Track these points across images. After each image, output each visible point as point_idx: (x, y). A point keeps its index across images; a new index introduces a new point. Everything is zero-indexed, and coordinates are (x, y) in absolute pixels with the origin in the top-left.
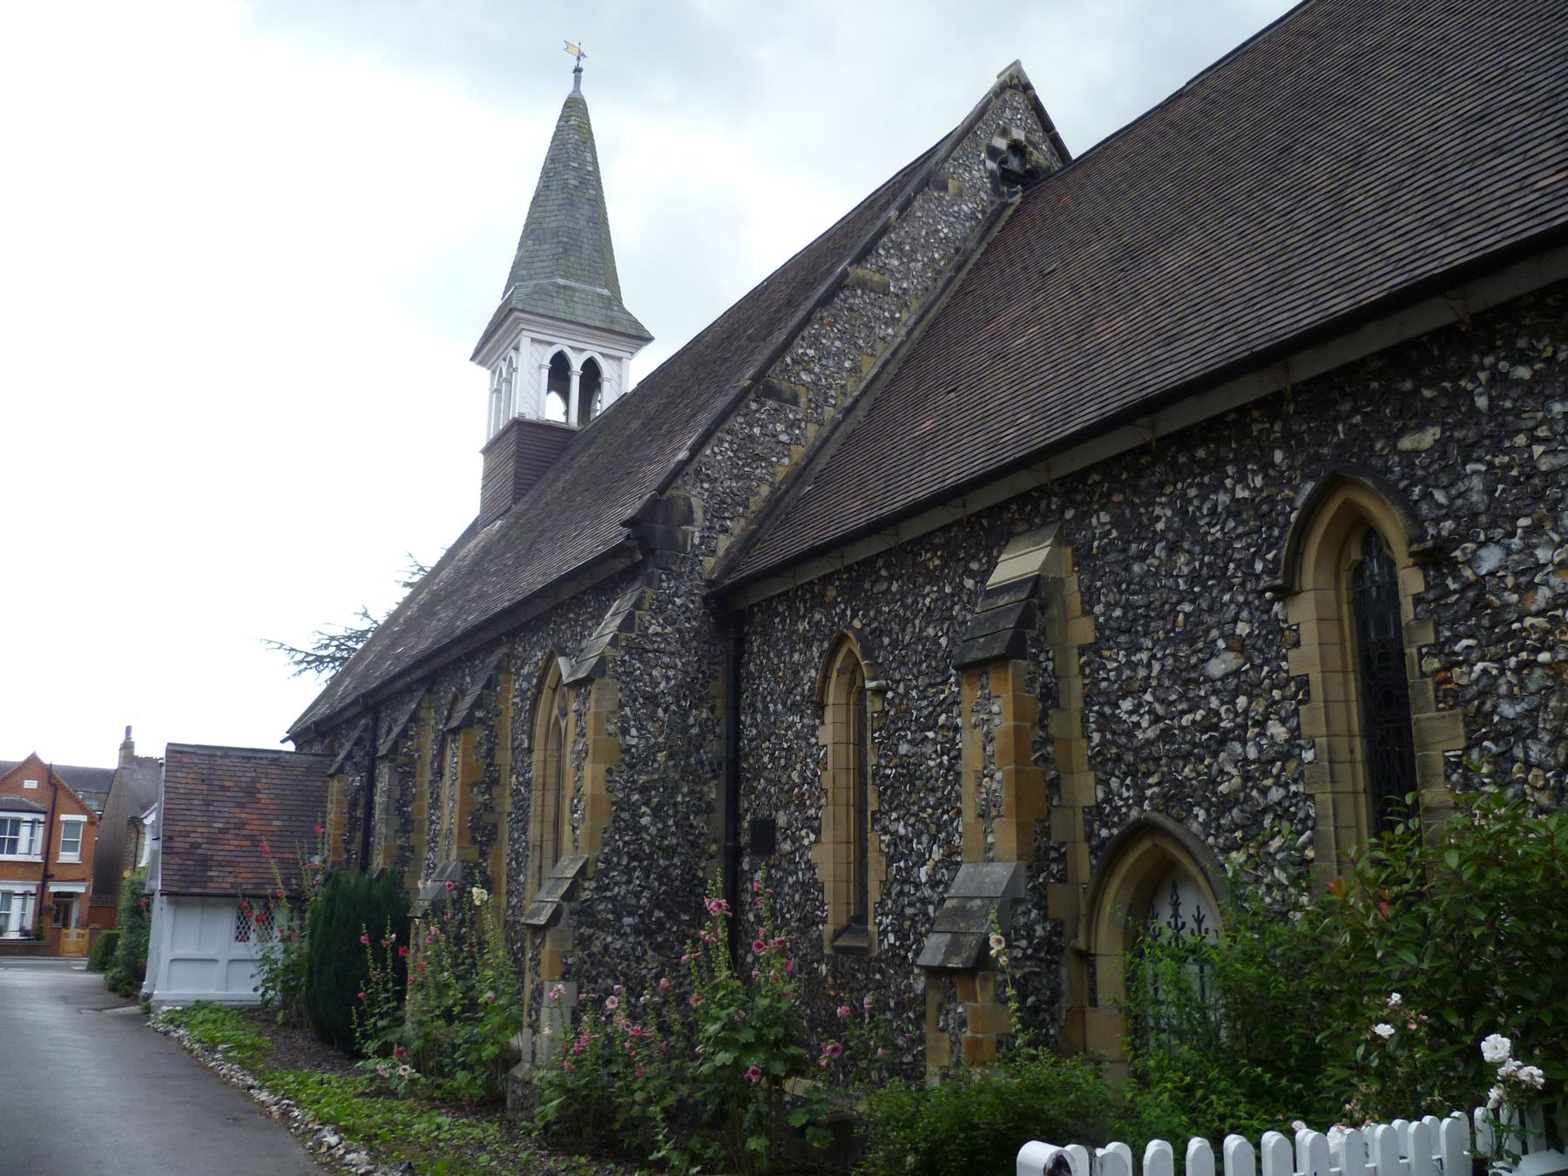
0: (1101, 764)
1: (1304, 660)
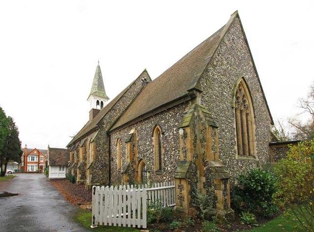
0: (139, 153)
1: (153, 143)
